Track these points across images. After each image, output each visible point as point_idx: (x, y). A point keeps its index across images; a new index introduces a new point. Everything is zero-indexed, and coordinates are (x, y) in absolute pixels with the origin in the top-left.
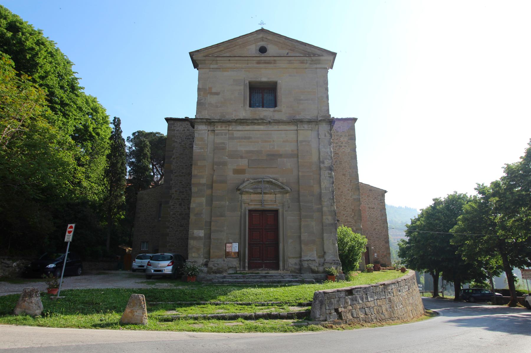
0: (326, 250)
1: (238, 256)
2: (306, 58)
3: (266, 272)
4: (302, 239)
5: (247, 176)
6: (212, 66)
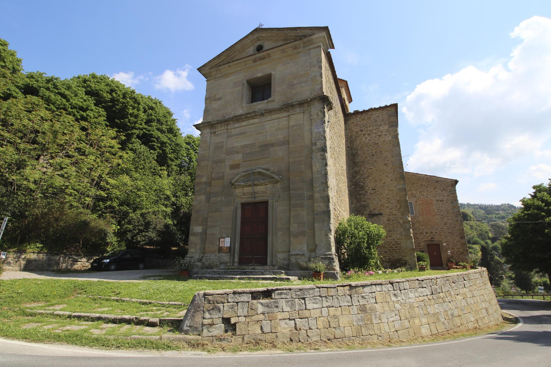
0: (317, 242)
1: (230, 250)
2: (297, 43)
3: (252, 267)
4: (291, 230)
5: (241, 169)
6: (218, 76)
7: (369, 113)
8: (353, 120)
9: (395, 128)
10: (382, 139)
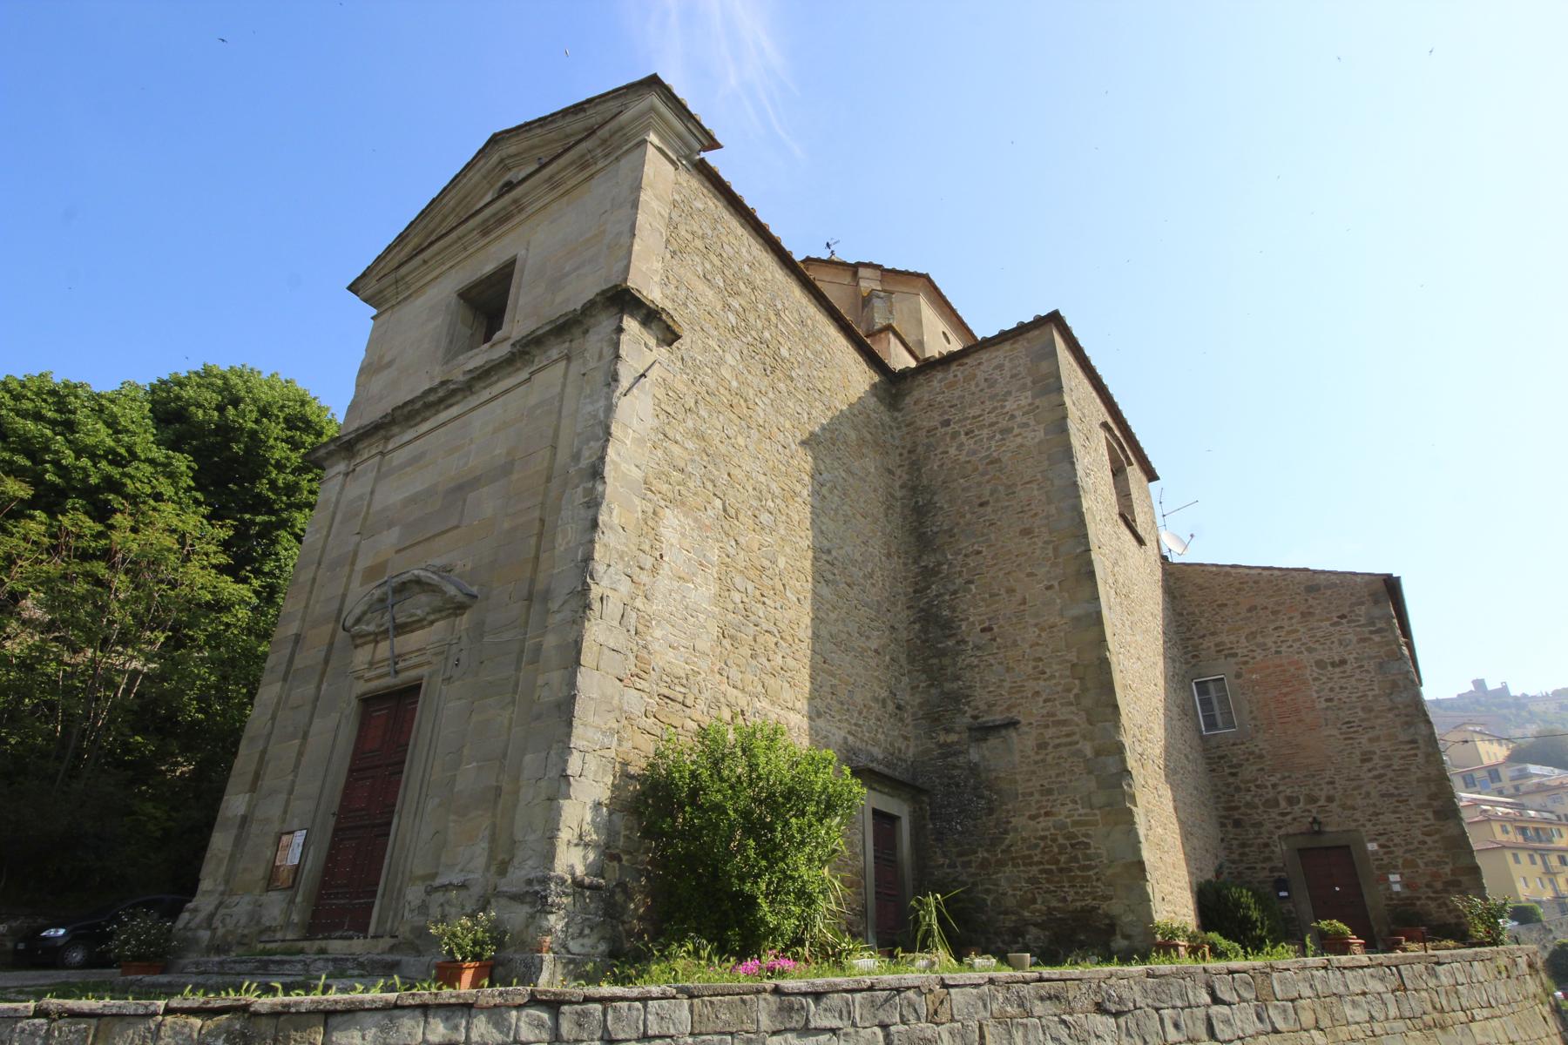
7: (969, 361)
8: (923, 392)
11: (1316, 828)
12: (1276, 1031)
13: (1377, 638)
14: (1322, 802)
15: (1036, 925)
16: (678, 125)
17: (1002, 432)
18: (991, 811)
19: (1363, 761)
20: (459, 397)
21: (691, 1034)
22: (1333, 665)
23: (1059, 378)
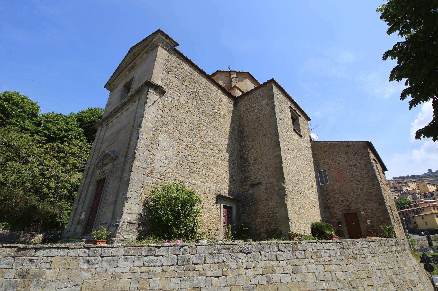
8: (242, 102)
9: (272, 100)
10: (262, 113)
11: (348, 208)
12: (298, 258)
13: (365, 158)
14: (350, 202)
15: (264, 233)
16: (167, 41)
17: (260, 110)
18: (255, 205)
19: (361, 190)
20: (120, 110)
21: (124, 256)
22: (353, 166)
23: (273, 95)
